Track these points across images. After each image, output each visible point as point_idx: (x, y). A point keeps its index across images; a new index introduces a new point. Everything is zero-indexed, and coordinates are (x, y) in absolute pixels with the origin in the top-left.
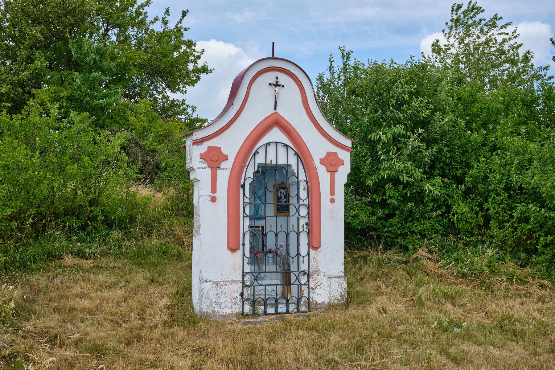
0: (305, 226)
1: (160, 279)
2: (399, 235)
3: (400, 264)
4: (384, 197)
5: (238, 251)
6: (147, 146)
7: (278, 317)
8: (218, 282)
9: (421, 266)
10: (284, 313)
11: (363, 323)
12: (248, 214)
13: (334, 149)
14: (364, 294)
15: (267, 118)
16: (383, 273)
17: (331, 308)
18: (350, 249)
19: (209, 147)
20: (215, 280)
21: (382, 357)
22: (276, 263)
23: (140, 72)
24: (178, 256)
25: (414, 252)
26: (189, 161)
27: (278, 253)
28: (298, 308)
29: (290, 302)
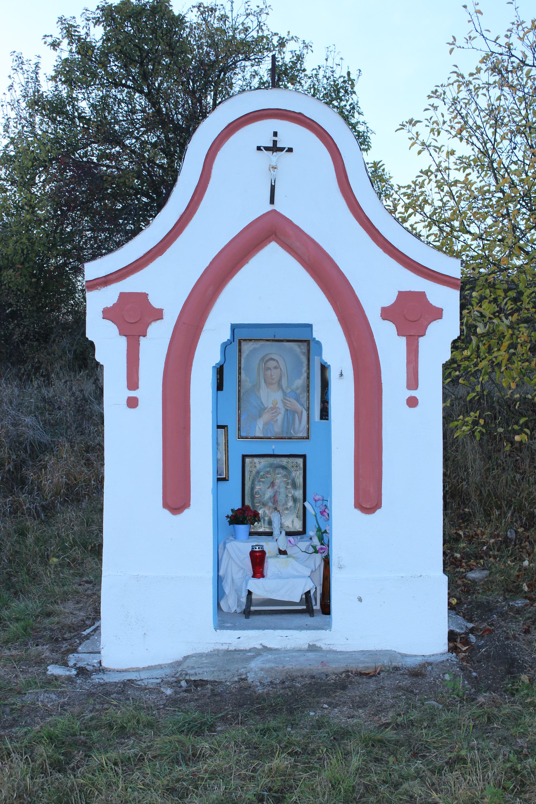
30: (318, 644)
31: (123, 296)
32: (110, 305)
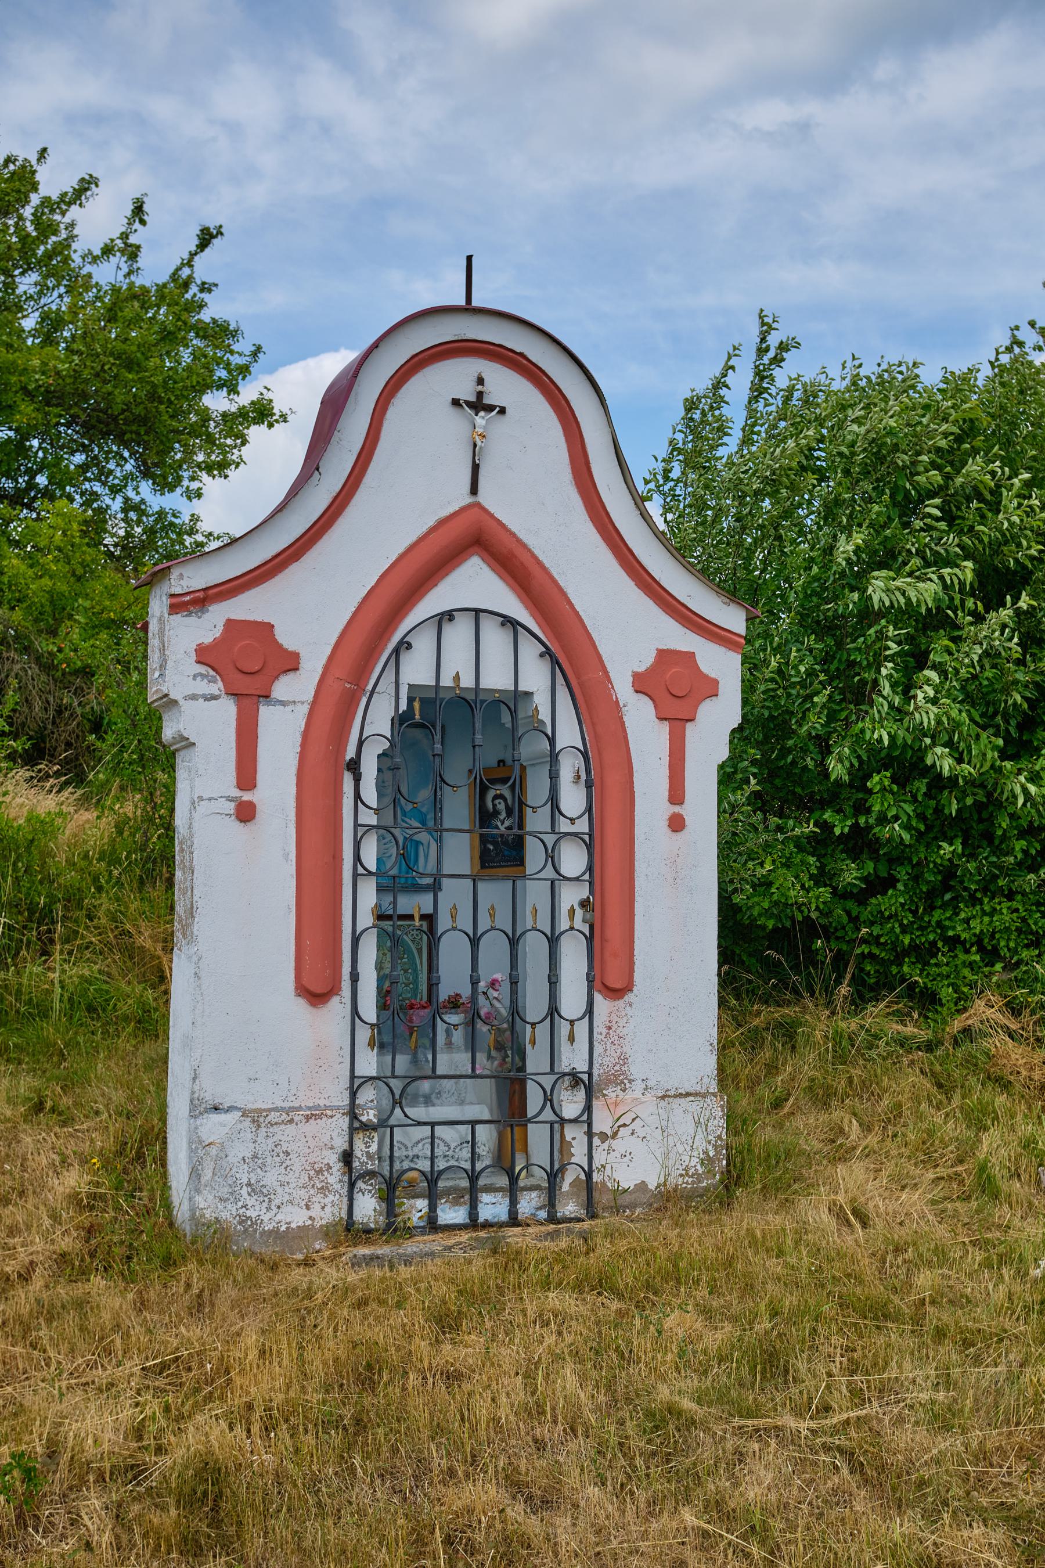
0: (579, 913)
1: (66, 1101)
2: (906, 952)
3: (909, 1051)
4: (862, 820)
5: (335, 1000)
6: (60, 656)
7: (476, 1239)
8: (259, 1111)
9: (983, 1058)
10: (501, 1225)
11: (786, 1264)
12: (371, 864)
13: (682, 639)
14: (788, 1155)
15: (442, 523)
16: (850, 1080)
17: (670, 1205)
18: (738, 998)
19: (230, 624)
20: (250, 1106)
21: (858, 1397)
22: (472, 1046)
23: (47, 414)
24: (139, 1022)
25: (958, 1011)
26: (157, 674)
27: (483, 1012)
28: (551, 1203)
29: (521, 1183)
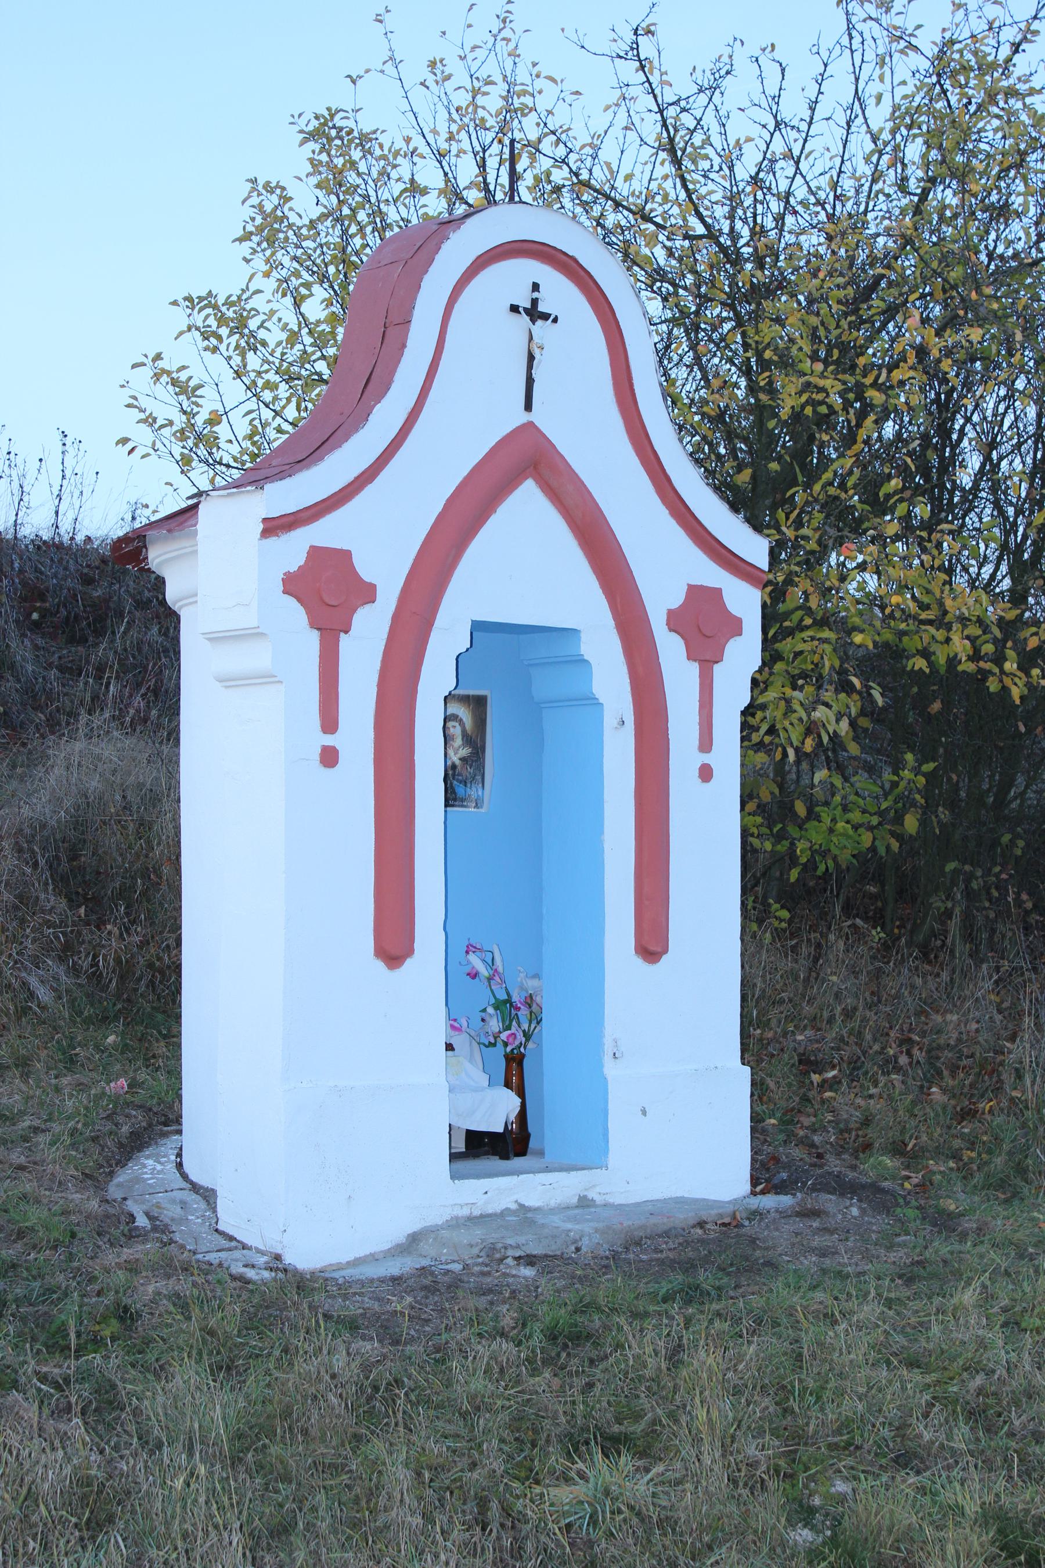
13: (713, 575)
30: (592, 1195)
31: (316, 553)
32: (293, 568)
